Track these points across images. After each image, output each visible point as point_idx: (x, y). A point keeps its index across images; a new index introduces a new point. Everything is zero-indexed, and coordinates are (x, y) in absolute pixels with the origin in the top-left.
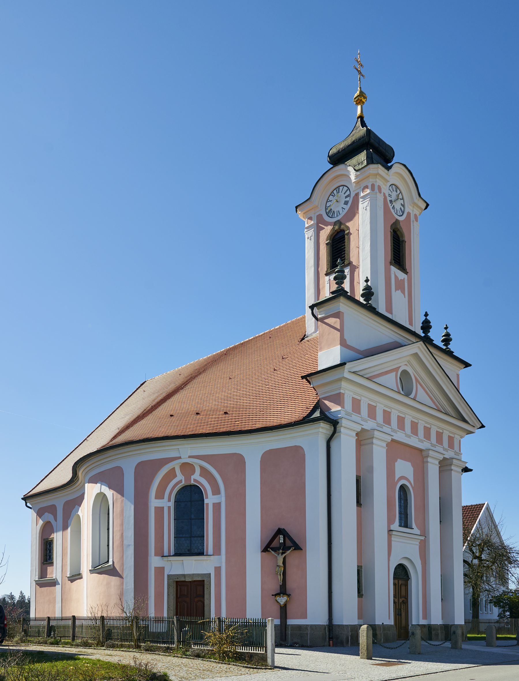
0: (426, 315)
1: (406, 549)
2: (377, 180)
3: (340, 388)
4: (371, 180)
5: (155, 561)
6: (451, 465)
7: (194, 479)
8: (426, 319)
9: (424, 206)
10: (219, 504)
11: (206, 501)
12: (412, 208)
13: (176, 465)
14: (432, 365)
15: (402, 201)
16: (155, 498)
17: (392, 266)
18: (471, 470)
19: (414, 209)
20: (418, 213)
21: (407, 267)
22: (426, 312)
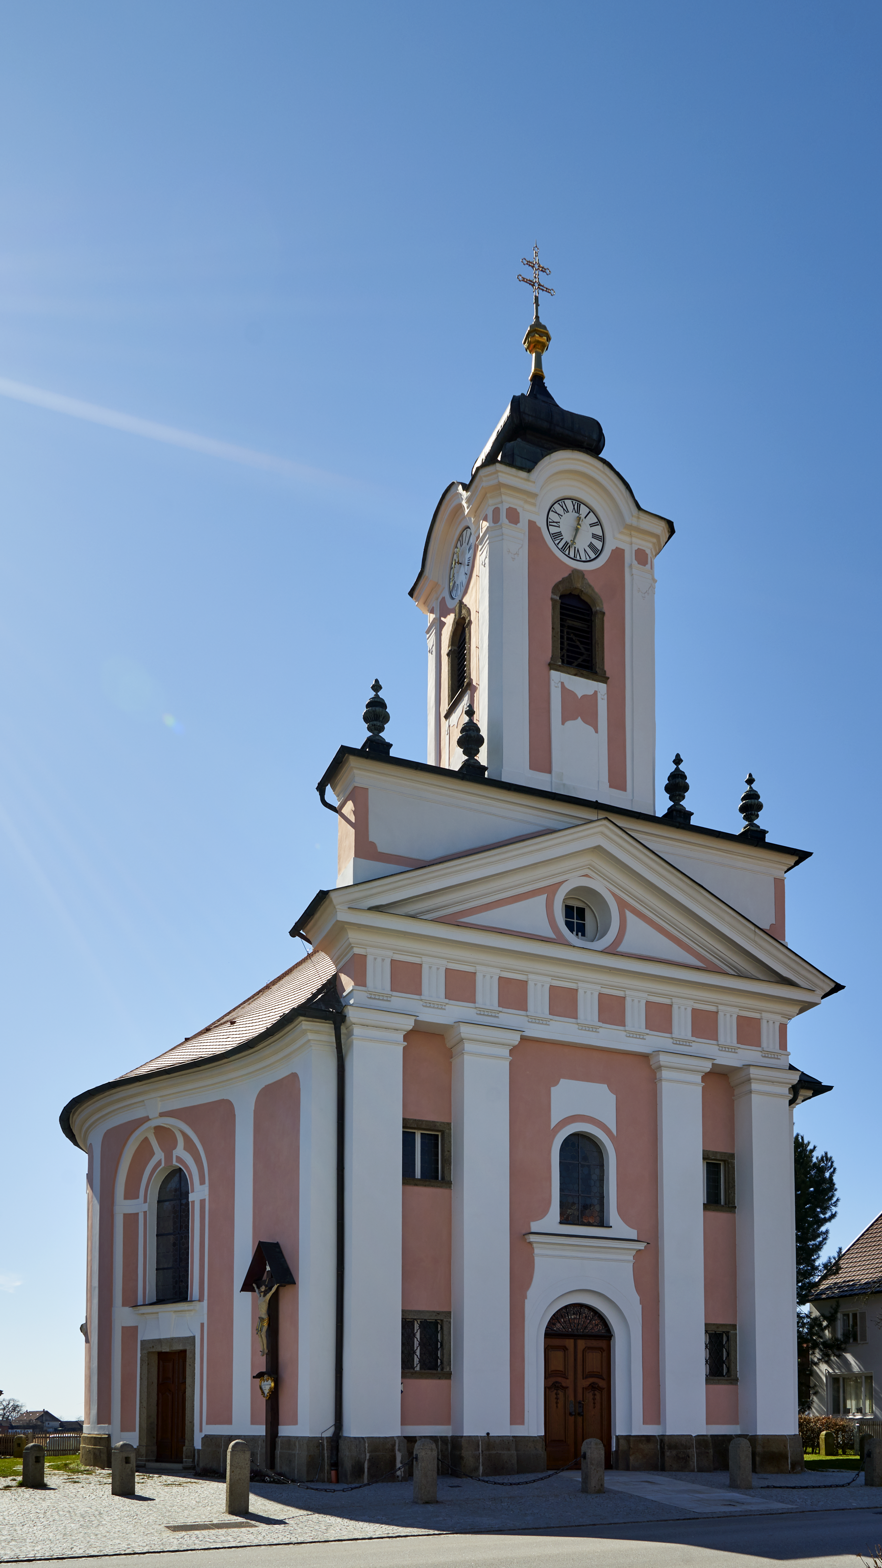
0: (678, 760)
1: (581, 1269)
2: (504, 497)
3: (350, 947)
4: (491, 501)
5: (123, 1317)
6: (749, 1080)
7: (177, 1157)
8: (677, 769)
9: (660, 529)
10: (127, 1197)
11: (192, 1197)
12: (627, 539)
13: (144, 1132)
14: (651, 868)
15: (597, 530)
16: (125, 1198)
17: (552, 672)
18: (829, 1088)
19: (634, 540)
20: (647, 546)
21: (609, 665)
22: (678, 755)
